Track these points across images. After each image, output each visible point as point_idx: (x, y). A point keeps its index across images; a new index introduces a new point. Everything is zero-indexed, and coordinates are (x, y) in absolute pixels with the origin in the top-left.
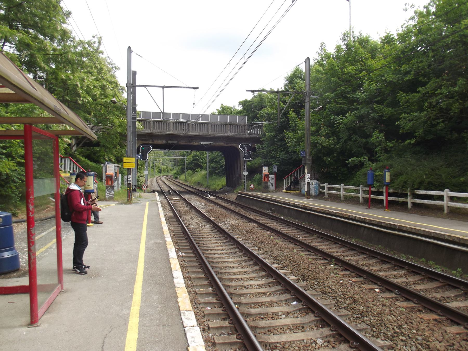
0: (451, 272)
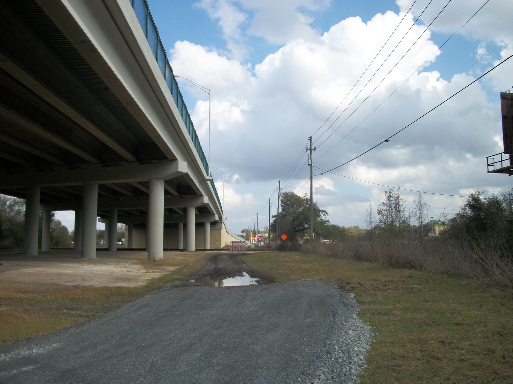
0: (50, 217)
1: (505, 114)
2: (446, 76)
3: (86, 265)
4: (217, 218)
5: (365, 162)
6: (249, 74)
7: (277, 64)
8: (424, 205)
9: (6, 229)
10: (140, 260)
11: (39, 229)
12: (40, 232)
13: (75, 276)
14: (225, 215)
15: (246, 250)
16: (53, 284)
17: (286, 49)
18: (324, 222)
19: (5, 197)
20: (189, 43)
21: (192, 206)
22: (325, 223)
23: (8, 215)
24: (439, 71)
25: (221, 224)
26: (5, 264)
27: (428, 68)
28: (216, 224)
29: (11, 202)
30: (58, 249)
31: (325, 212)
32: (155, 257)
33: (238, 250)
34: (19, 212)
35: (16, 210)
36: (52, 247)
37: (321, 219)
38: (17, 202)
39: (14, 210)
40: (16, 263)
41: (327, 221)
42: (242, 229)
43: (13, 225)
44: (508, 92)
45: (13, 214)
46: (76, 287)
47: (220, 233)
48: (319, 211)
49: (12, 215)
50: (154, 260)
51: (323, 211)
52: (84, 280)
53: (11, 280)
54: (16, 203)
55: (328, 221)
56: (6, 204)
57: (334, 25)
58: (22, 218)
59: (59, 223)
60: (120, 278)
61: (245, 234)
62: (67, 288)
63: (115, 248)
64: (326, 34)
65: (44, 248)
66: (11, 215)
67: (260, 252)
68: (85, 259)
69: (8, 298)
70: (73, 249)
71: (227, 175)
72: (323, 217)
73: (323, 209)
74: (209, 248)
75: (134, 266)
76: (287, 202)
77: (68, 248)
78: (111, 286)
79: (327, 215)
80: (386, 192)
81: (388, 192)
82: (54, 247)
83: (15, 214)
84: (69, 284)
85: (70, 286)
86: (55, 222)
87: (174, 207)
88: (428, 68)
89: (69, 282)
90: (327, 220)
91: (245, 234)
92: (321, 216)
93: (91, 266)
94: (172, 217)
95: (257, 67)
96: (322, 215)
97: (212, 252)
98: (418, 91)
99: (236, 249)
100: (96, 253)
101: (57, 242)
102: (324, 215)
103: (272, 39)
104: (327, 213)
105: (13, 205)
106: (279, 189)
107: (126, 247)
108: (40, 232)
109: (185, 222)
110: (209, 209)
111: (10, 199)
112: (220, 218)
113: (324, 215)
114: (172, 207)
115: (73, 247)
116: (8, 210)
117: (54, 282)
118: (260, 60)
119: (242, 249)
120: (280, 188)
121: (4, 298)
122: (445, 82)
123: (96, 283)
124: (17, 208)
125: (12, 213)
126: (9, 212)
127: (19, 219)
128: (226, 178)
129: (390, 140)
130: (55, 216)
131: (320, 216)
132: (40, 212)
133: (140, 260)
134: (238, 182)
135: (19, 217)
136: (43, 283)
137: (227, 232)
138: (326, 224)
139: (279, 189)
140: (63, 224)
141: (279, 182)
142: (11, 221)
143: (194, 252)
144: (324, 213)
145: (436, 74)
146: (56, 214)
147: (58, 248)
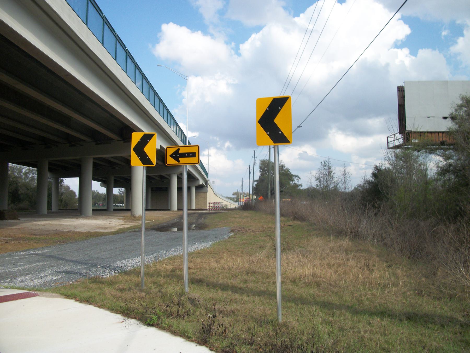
0: (58, 184)
1: (400, 104)
2: (414, 53)
3: (82, 220)
4: (201, 182)
5: (343, 130)
6: (233, 52)
7: (258, 44)
8: (348, 173)
9: (22, 193)
10: (124, 216)
11: (92, 194)
12: (50, 196)
13: (70, 226)
14: (211, 180)
15: (220, 210)
16: (54, 231)
17: (265, 30)
18: (297, 186)
19: (21, 167)
20: (179, 26)
21: (174, 174)
22: (298, 187)
23: (23, 181)
24: (409, 48)
25: (207, 188)
26: (22, 220)
27: (398, 45)
28: (201, 189)
29: (26, 170)
30: (67, 210)
31: (298, 177)
32: (135, 214)
33: (216, 210)
34: (33, 178)
35: (30, 177)
36: (61, 208)
37: (295, 183)
38: (31, 170)
39: (29, 177)
40: (30, 219)
41: (300, 185)
42: (233, 192)
43: (29, 190)
44: (401, 86)
45: (28, 180)
46: (69, 232)
47: (206, 195)
48: (292, 176)
49: (28, 182)
50: (135, 217)
51: (296, 176)
52: (75, 228)
53: (26, 228)
54: (30, 171)
55: (301, 185)
56: (22, 172)
57: (305, 10)
58: (35, 183)
59: (68, 188)
60: (101, 227)
61: (235, 196)
62: (63, 233)
63: (112, 208)
64: (302, 15)
65: (54, 208)
66: (26, 181)
67: (227, 211)
68: (83, 216)
69: (25, 238)
70: (77, 210)
71: (219, 143)
72: (296, 181)
73: (297, 175)
74: (194, 208)
75: (116, 221)
76: (265, 168)
77: (74, 209)
78: (92, 231)
79: (299, 179)
80: (321, 163)
81: (323, 162)
82: (64, 209)
83: (30, 180)
84: (65, 230)
85: (65, 231)
86: (64, 187)
87: (163, 174)
88: (398, 45)
89: (65, 229)
90: (300, 184)
91: (235, 196)
92: (294, 180)
93: (84, 220)
94: (163, 181)
95: (241, 46)
96: (295, 180)
97: (192, 211)
98: (387, 65)
99: (215, 209)
100: (92, 213)
101: (66, 205)
102: (297, 179)
103: (250, 22)
104: (300, 178)
105: (28, 173)
106: (254, 158)
107: (125, 208)
108: (50, 196)
109: (181, 186)
110: (193, 176)
111: (25, 169)
112: (206, 182)
113: (297, 179)
114: (161, 174)
115: (77, 208)
116: (23, 177)
117: (55, 229)
118: (244, 39)
119: (217, 209)
120: (255, 157)
121: (22, 238)
122: (413, 58)
123: (82, 230)
124: (31, 175)
125: (27, 179)
126: (24, 179)
127: (33, 184)
128: (218, 146)
129: (302, 126)
130: (64, 181)
131: (293, 180)
132: (49, 178)
133: (124, 216)
134: (229, 149)
135: (33, 183)
136: (48, 230)
137: (215, 195)
138: (299, 188)
139: (254, 158)
140: (72, 188)
141: (255, 151)
142: (26, 186)
143: (176, 211)
144: (297, 178)
145: (406, 51)
146: (65, 180)
147: (67, 209)
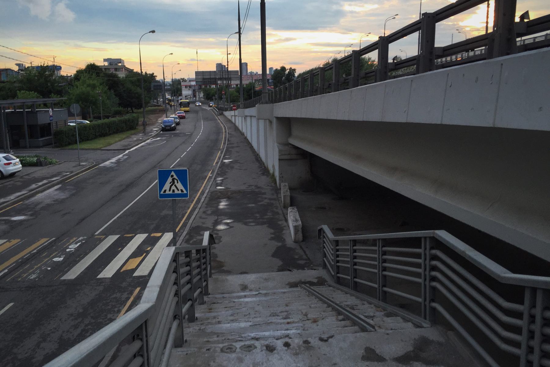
0: (268, 74)
